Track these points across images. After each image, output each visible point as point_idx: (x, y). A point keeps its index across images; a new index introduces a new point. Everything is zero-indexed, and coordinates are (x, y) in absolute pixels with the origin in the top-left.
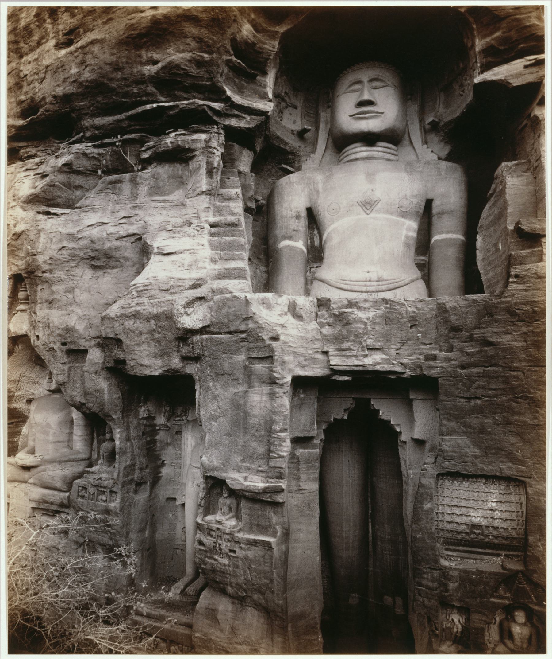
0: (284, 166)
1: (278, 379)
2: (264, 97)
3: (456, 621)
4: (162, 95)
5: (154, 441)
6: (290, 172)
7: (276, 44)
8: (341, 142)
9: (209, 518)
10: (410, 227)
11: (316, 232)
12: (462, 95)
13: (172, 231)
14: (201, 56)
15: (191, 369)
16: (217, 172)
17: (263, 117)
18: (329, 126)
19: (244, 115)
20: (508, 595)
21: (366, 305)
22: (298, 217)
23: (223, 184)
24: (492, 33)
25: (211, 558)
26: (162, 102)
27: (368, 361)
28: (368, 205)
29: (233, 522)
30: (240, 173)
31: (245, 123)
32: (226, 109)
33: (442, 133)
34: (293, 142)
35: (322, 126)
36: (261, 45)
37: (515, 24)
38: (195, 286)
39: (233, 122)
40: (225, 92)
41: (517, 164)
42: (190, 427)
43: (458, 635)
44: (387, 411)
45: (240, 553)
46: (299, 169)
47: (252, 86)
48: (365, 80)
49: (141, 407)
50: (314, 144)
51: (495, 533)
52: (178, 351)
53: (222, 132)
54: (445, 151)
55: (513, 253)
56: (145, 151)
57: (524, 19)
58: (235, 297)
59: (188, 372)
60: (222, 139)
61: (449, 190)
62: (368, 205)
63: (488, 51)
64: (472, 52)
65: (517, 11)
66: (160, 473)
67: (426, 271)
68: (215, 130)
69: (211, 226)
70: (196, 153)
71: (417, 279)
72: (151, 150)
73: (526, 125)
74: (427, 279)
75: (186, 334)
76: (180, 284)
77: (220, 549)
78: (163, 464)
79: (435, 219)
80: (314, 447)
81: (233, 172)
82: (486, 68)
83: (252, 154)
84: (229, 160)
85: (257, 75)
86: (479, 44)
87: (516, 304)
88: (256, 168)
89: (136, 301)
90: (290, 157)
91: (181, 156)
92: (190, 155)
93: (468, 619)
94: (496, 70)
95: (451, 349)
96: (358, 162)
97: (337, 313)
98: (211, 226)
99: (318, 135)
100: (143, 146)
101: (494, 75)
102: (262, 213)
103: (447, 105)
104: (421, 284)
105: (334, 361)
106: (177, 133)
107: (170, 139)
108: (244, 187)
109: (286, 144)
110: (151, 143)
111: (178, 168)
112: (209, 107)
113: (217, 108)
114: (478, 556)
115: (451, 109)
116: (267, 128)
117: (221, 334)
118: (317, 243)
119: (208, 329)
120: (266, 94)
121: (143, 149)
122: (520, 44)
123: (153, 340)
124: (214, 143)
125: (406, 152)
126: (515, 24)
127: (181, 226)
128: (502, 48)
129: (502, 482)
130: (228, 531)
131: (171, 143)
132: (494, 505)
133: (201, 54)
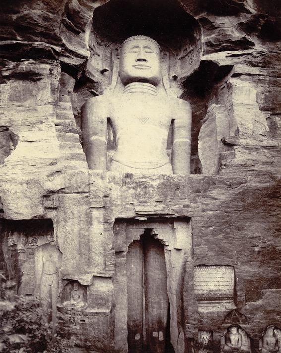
0: (93, 90)
1: (109, 219)
2: (84, 46)
3: (205, 338)
4: (19, 36)
5: (17, 260)
6: (96, 95)
7: (92, 14)
8: (127, 81)
9: (65, 303)
10: (165, 133)
11: (111, 132)
12: (190, 64)
13: (30, 126)
14: (47, 14)
15: (51, 215)
16: (57, 91)
17: (85, 60)
18: (119, 69)
19: (73, 57)
20: (229, 321)
21: (154, 178)
22: (102, 123)
23: (60, 99)
24: (210, 35)
25: (68, 326)
26: (19, 40)
27: (155, 209)
28: (144, 120)
29: (82, 304)
30: (69, 92)
31: (73, 61)
32: (63, 52)
33: (179, 83)
34: (96, 77)
35: (115, 69)
36: (83, 14)
37: (222, 32)
38: (52, 164)
39: (66, 60)
40: (62, 40)
41: (220, 107)
42: (41, 249)
43: (206, 344)
44: (161, 233)
45: (87, 321)
46: (101, 93)
47: (77, 38)
48: (141, 46)
49: (10, 239)
50: (110, 79)
51: (220, 293)
52: (42, 204)
53: (60, 65)
54: (181, 92)
55: (222, 153)
56: (6, 71)
57: (226, 30)
58: (81, 171)
59: (48, 216)
60: (60, 69)
61: (183, 112)
62: (144, 120)
63: (209, 44)
64: (199, 42)
65: (223, 25)
66: (21, 279)
67: (172, 157)
68: (55, 64)
69: (56, 125)
70: (43, 77)
71: (168, 163)
72: (11, 71)
73: (224, 87)
74: (172, 161)
75: (49, 193)
76: (43, 162)
77: (74, 321)
78: (23, 274)
79: (176, 130)
80: (124, 257)
81: (65, 91)
82: (206, 52)
83: (75, 80)
84: (63, 83)
85: (80, 33)
86: (204, 39)
87: (226, 179)
88: (77, 88)
89: (11, 171)
90: (95, 85)
91: (32, 77)
92: (38, 77)
93: (212, 336)
94: (212, 55)
95: (196, 202)
96: (136, 93)
97: (138, 182)
98: (56, 125)
99: (112, 75)
100: (5, 67)
101: (211, 57)
102: (81, 116)
103: (182, 68)
104: (170, 165)
105: (138, 209)
106: (28, 62)
107: (25, 65)
108: (72, 101)
109: (93, 76)
110: (11, 67)
111: (30, 85)
112: (52, 48)
113: (57, 50)
114: (213, 305)
115: (186, 70)
116: (86, 66)
117: (72, 193)
118: (112, 138)
119: (64, 191)
120: (85, 45)
121: (4, 69)
122: (223, 43)
123: (26, 197)
124: (55, 72)
125: (160, 90)
126: (222, 32)
127: (35, 124)
128: (215, 43)
129: (223, 267)
130: (79, 310)
131: (26, 68)
132: (219, 279)
133: (47, 13)
